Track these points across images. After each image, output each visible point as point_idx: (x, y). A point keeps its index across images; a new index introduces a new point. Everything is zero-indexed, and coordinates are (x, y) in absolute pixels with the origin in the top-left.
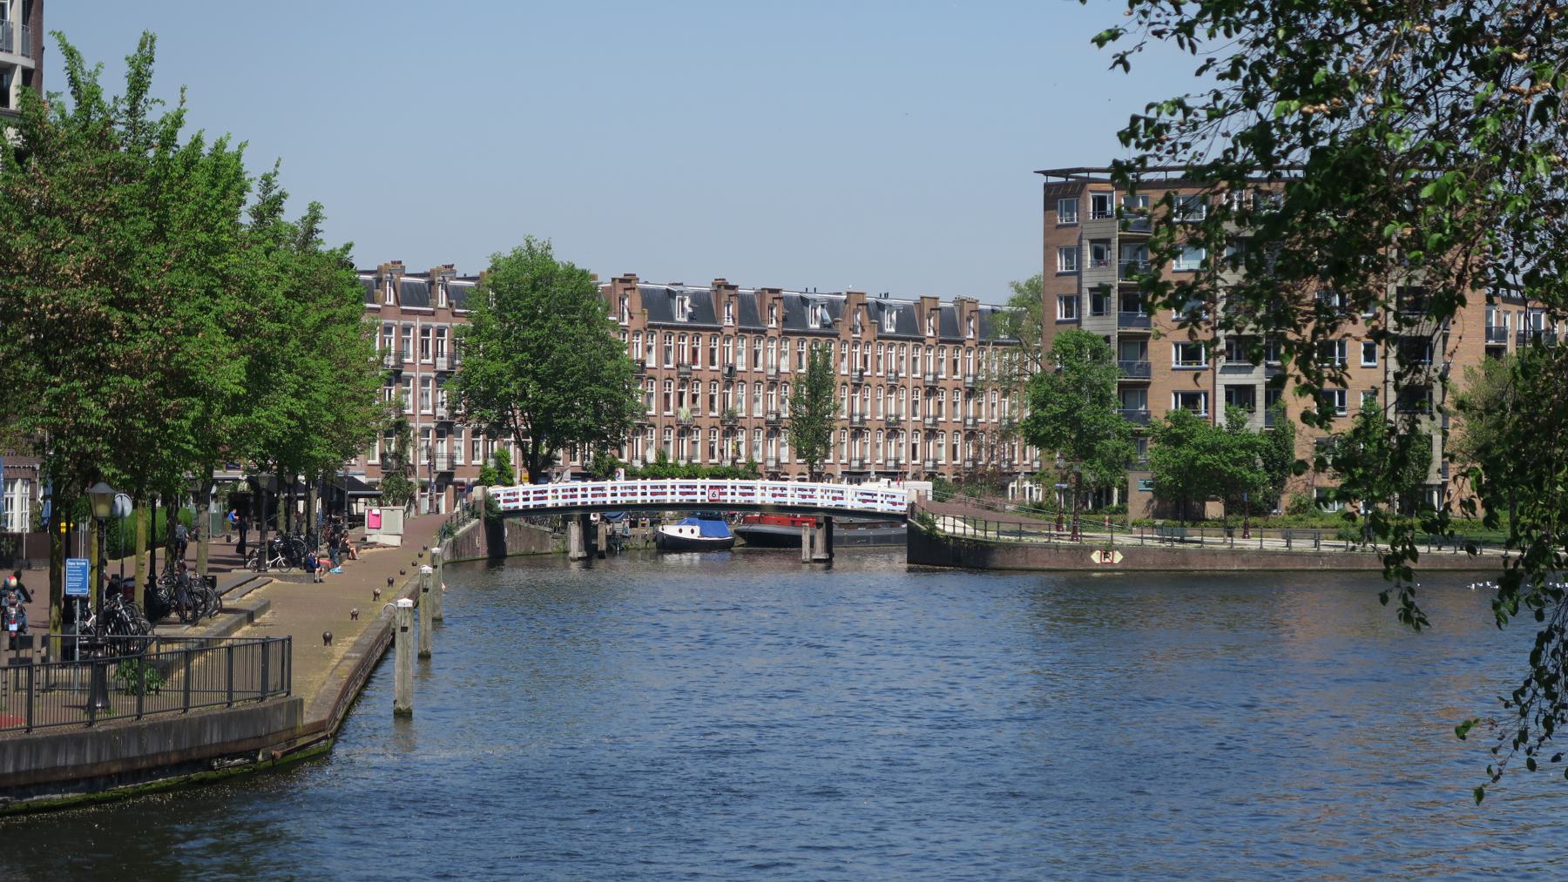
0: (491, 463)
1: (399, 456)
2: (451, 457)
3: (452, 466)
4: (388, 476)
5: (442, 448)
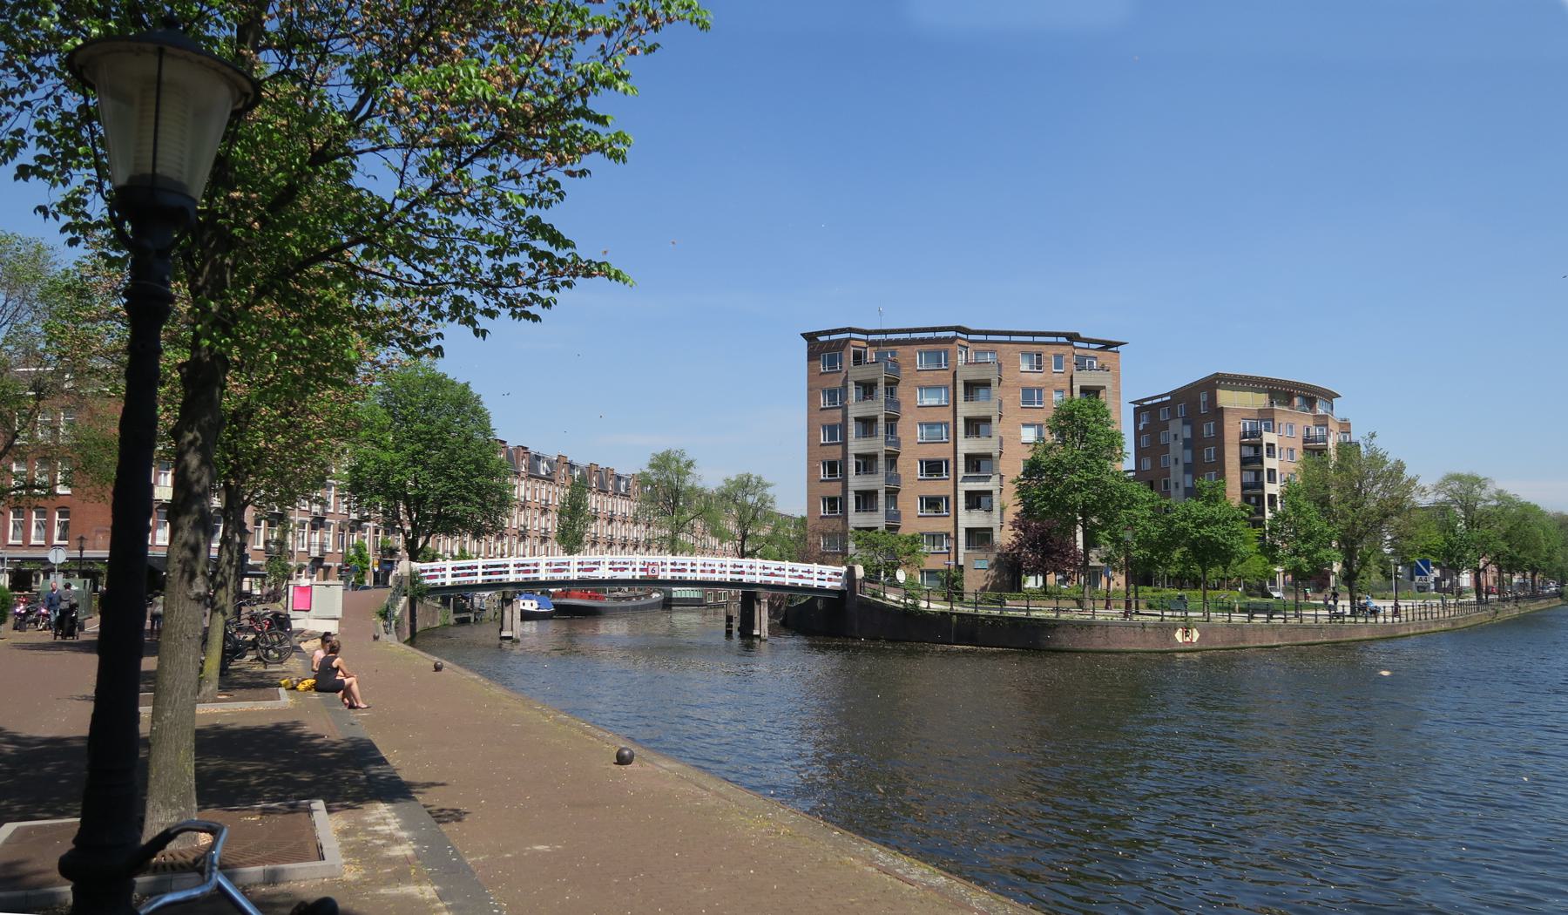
0: (352, 552)
1: (281, 543)
2: (322, 545)
3: (323, 553)
4: (271, 559)
5: (316, 538)
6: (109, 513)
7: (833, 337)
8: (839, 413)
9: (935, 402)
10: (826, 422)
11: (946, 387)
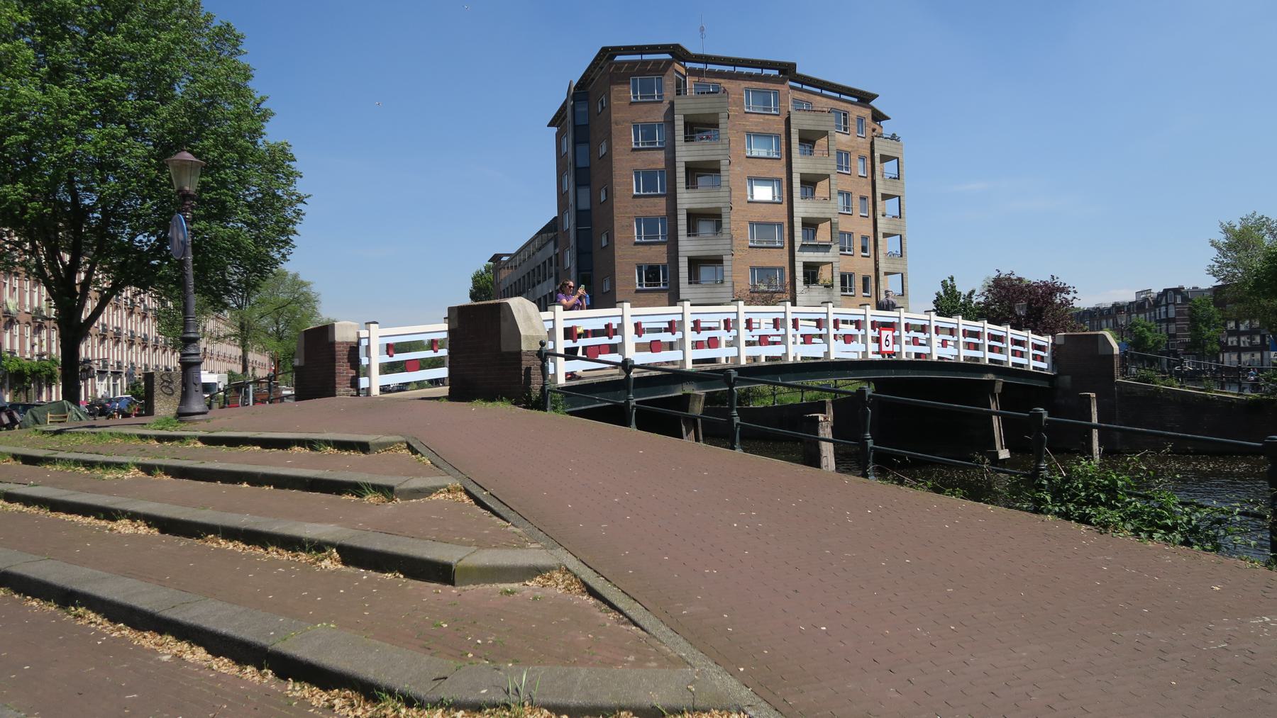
6: (146, 607)
7: (646, 57)
8: (661, 155)
9: (763, 153)
10: (639, 165)
11: (778, 137)
